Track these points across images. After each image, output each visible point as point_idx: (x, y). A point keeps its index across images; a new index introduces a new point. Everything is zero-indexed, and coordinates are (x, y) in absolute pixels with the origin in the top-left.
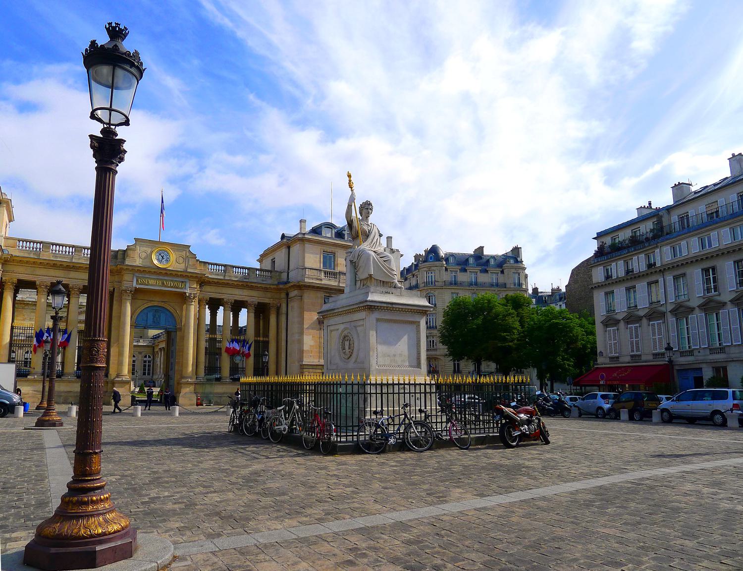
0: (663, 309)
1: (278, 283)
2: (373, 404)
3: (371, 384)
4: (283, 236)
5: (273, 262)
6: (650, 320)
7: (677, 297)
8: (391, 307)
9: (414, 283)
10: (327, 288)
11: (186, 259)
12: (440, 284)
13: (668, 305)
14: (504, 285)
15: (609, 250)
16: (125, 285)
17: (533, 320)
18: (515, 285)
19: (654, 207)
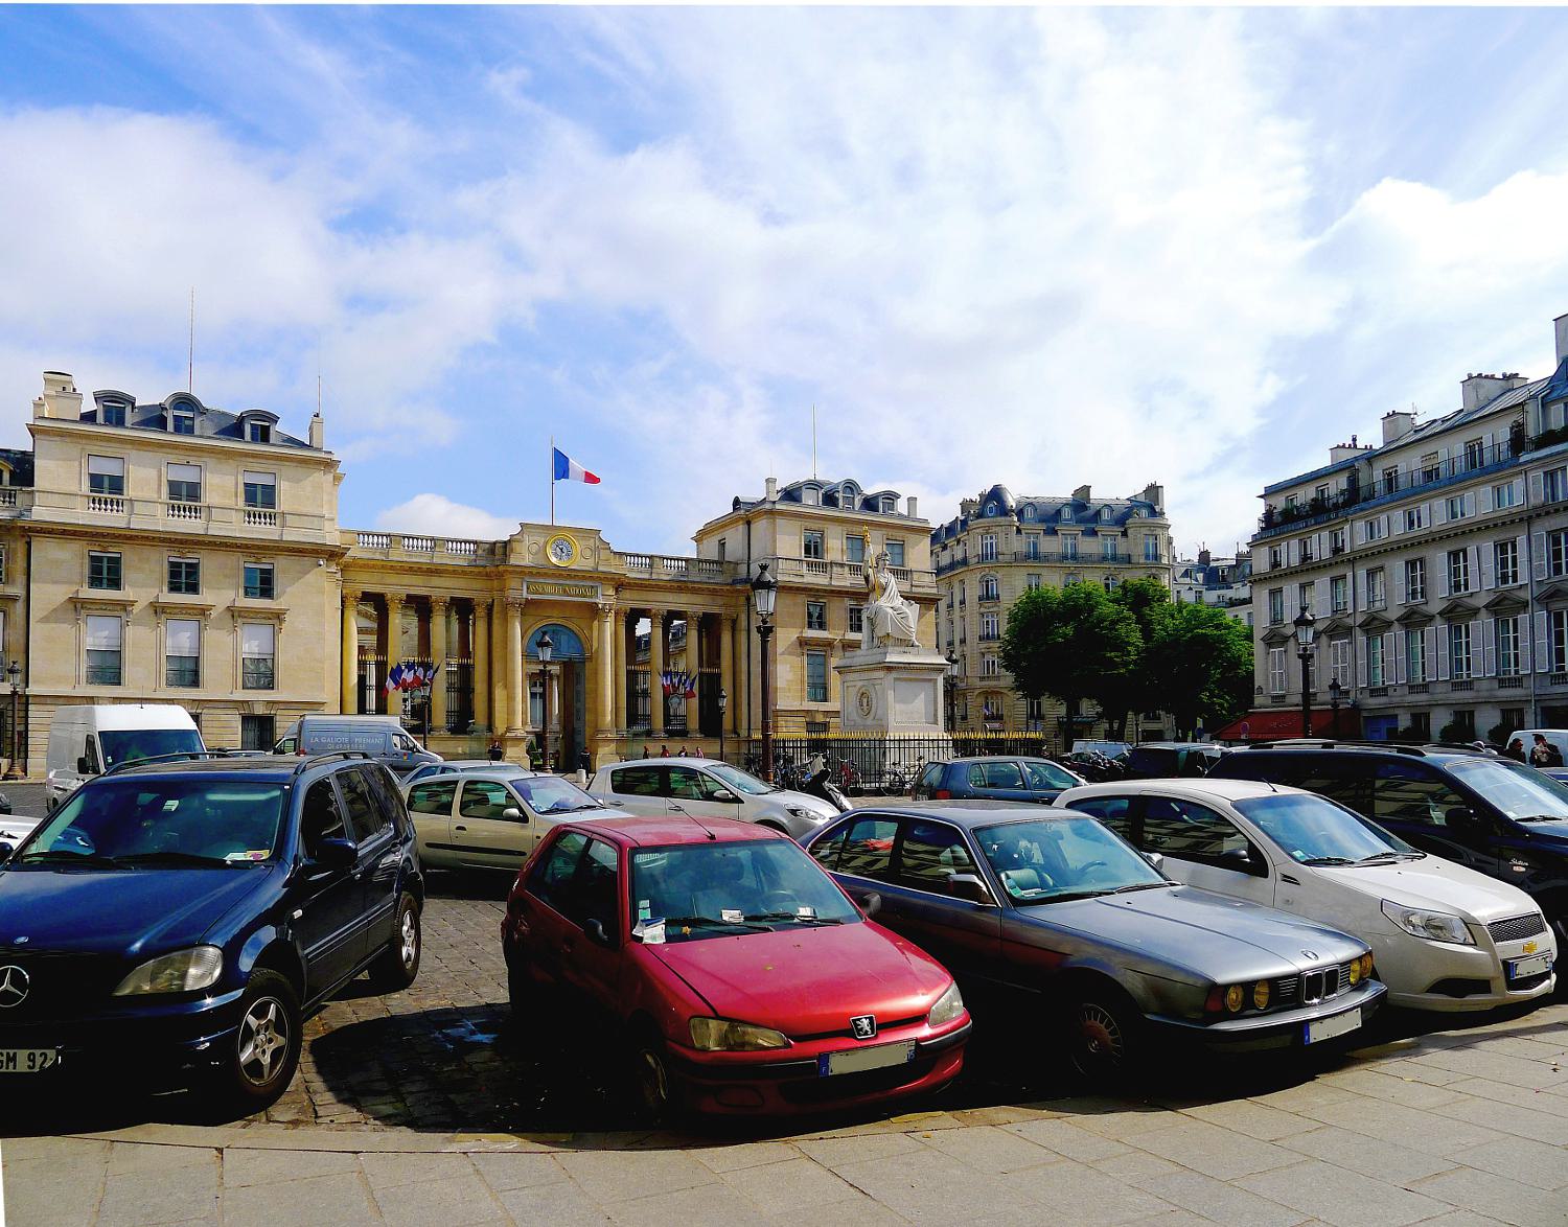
0: (1350, 621)
1: (733, 581)
2: (892, 756)
3: (890, 740)
4: (737, 502)
5: (722, 545)
6: (1331, 638)
7: (1371, 602)
8: (908, 667)
9: (959, 556)
10: (811, 590)
11: (595, 550)
12: (1007, 558)
13: (1358, 615)
14: (1128, 559)
15: (1280, 519)
16: (512, 594)
17: (1165, 629)
18: (1147, 557)
19: (1360, 445)
